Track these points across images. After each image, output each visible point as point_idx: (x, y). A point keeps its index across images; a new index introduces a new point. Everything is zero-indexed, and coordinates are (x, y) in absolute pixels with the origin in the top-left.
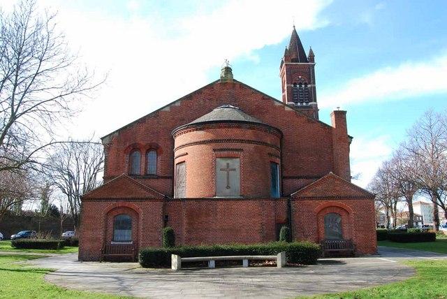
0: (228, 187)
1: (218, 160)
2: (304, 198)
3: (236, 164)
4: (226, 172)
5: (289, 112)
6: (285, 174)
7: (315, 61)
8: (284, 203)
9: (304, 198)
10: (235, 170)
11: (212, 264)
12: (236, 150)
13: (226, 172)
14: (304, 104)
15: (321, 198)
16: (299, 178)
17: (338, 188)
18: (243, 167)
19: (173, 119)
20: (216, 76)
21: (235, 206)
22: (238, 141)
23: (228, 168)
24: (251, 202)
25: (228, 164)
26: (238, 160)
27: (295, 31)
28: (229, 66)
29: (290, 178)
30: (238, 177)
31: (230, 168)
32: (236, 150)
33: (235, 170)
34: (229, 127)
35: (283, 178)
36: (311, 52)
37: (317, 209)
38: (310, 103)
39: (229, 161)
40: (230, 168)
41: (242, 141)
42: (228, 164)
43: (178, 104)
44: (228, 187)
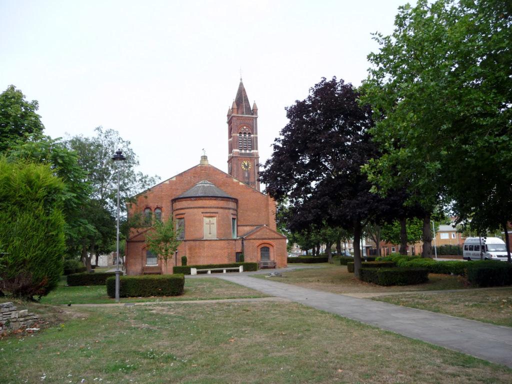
0: (210, 234)
1: (204, 218)
2: (250, 239)
3: (214, 220)
4: (209, 225)
5: (242, 186)
6: (239, 224)
7: (258, 114)
8: (240, 242)
9: (250, 239)
10: (213, 224)
11: (225, 271)
12: (215, 213)
13: (209, 225)
14: (248, 151)
15: (259, 239)
16: (246, 226)
17: (268, 234)
18: (218, 222)
19: (171, 189)
20: (196, 162)
21: (214, 243)
22: (215, 208)
23: (210, 223)
24: (222, 242)
25: (210, 221)
26: (216, 218)
27: (241, 84)
28: (206, 155)
29: (242, 226)
30: (216, 227)
31: (211, 222)
32: (215, 213)
33: (213, 224)
34: (211, 200)
35: (238, 226)
36: (255, 105)
37: (257, 244)
38: (252, 151)
39: (211, 219)
40: (211, 222)
41: (218, 208)
42: (210, 221)
43: (174, 179)
44: (210, 234)
